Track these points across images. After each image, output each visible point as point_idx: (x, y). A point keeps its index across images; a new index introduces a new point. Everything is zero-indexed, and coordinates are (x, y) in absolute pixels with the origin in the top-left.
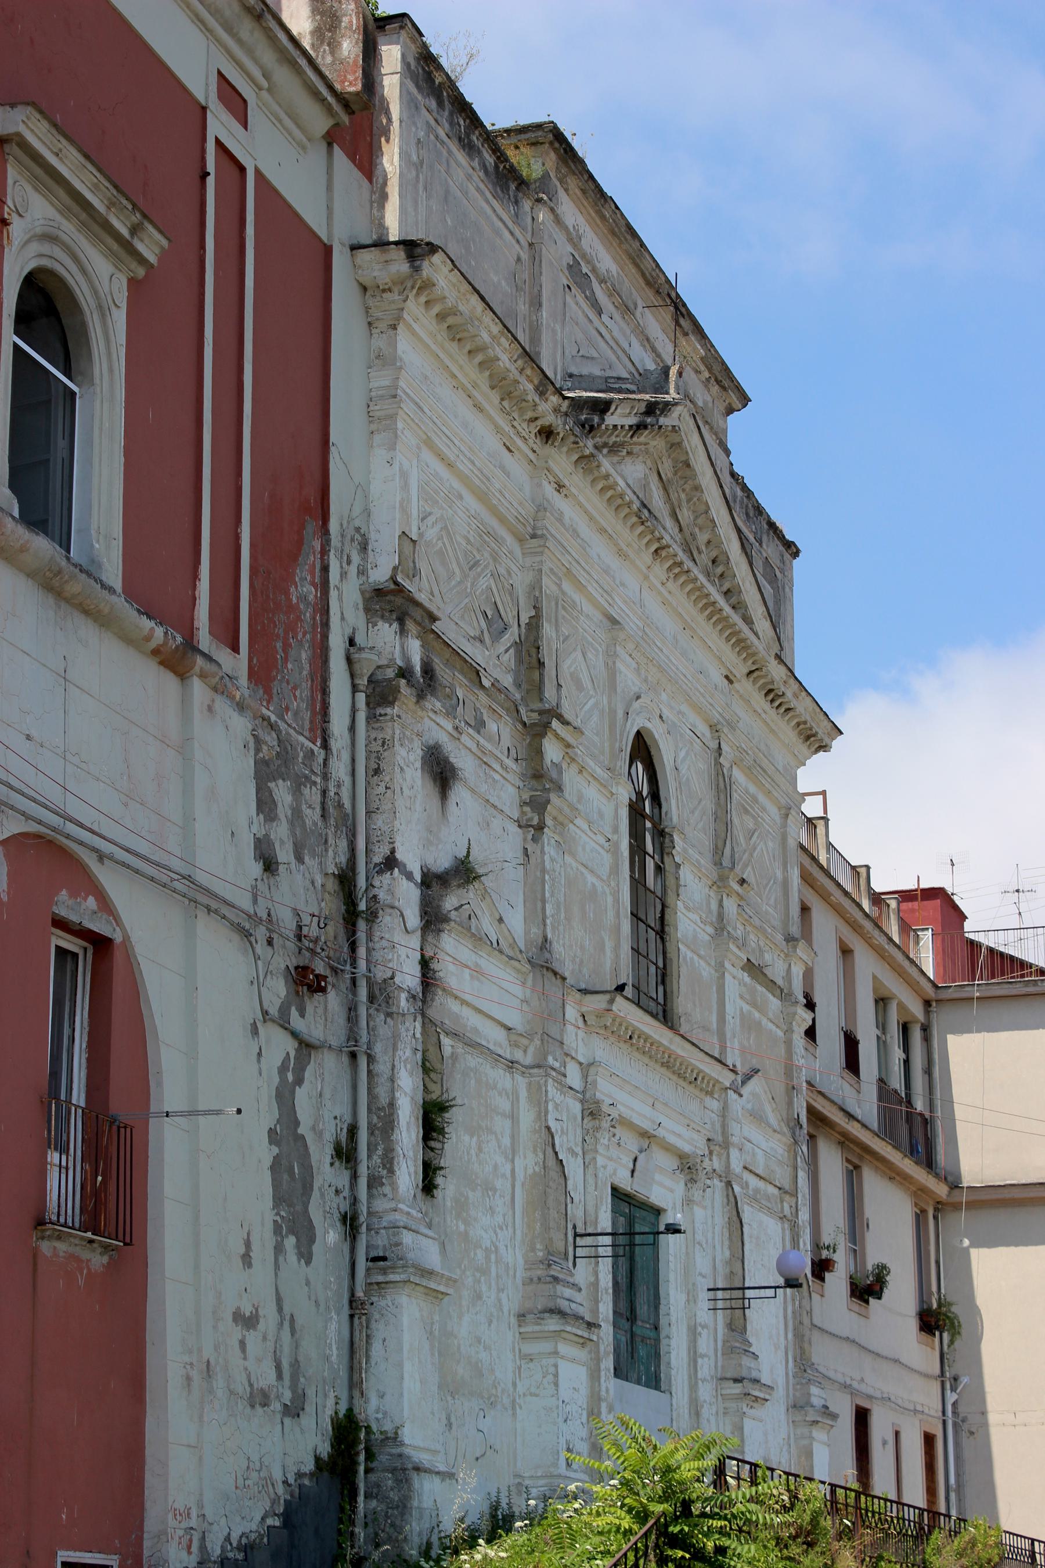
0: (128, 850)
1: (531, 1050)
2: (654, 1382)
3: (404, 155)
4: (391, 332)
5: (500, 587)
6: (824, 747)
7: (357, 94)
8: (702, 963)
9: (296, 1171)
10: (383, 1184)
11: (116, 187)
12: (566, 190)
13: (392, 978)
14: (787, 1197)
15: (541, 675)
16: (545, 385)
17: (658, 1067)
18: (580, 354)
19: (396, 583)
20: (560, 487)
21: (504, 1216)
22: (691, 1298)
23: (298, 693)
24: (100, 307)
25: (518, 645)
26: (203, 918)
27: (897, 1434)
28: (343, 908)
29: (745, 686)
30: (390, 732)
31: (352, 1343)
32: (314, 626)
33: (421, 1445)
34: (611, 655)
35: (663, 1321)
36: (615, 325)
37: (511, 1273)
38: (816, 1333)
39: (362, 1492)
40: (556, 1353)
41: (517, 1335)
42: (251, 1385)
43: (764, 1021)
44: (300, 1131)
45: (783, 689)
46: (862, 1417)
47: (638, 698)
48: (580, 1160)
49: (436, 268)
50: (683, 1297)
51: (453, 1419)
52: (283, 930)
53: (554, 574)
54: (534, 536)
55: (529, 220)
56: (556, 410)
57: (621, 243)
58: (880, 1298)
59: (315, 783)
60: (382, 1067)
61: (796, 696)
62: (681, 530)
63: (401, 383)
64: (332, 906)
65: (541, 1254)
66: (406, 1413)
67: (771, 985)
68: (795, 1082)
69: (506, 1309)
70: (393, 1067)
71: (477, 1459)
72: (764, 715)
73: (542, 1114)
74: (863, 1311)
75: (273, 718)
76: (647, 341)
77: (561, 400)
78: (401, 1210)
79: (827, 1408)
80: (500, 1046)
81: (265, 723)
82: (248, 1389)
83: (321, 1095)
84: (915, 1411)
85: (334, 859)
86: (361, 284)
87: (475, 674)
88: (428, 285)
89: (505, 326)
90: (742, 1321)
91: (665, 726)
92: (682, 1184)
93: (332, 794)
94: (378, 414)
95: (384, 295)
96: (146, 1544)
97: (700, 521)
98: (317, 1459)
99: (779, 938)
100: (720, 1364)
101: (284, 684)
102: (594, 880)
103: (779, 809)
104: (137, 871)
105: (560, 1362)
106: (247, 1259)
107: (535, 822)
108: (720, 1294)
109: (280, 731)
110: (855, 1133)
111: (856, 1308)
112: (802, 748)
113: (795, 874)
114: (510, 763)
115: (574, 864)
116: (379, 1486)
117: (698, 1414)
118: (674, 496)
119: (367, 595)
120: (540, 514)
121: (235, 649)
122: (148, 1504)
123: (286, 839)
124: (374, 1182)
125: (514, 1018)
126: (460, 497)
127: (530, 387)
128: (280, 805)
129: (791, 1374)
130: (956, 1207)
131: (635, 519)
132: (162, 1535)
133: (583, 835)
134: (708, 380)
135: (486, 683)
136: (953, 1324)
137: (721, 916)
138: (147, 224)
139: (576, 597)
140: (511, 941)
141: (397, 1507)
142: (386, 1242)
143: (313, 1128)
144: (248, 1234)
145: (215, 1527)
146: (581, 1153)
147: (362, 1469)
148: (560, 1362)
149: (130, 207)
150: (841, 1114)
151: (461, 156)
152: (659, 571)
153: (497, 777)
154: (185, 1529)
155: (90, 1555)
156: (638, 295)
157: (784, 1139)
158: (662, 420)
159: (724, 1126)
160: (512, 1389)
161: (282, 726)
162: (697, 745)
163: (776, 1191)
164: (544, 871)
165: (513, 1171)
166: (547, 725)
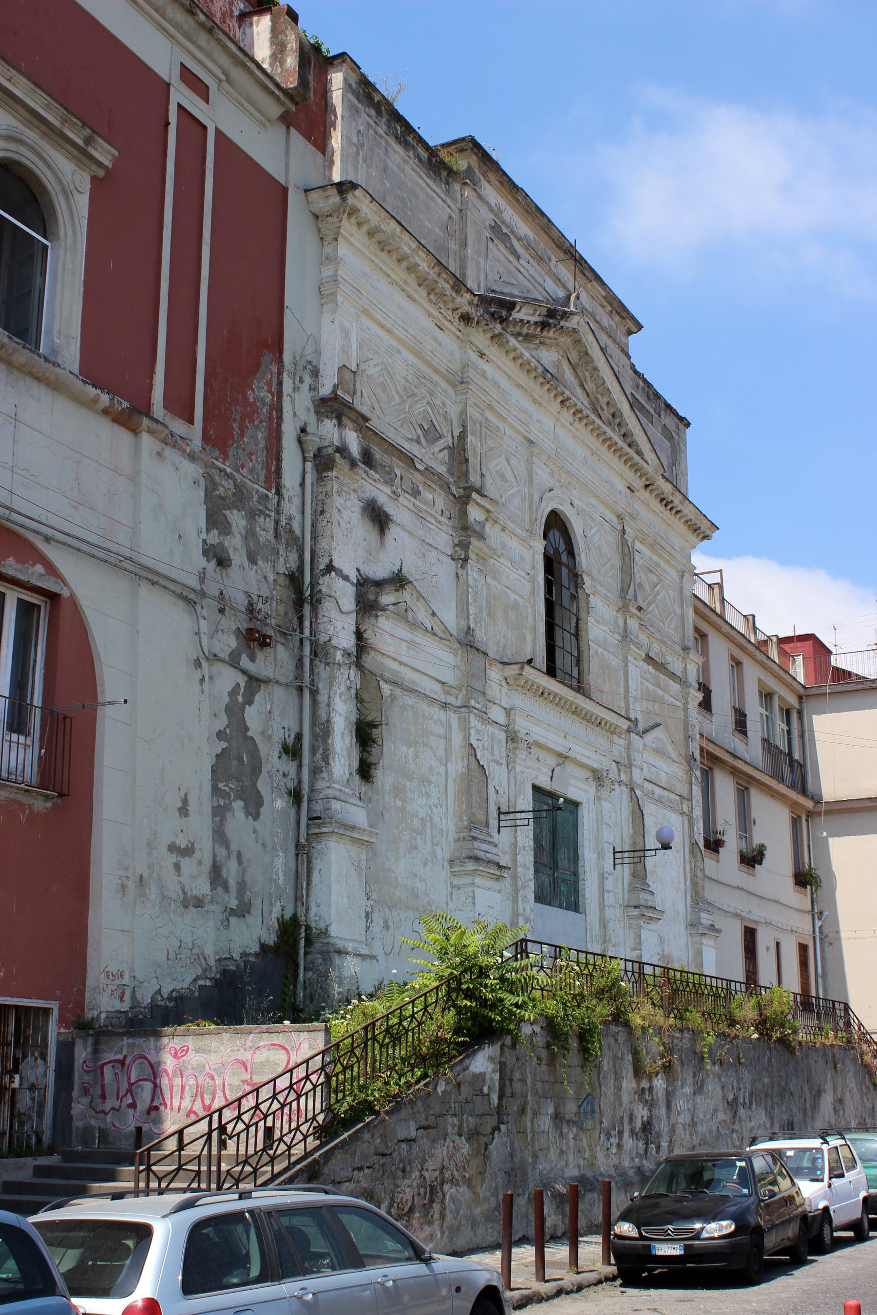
0: (66, 534)
1: (460, 697)
2: (574, 906)
3: (346, 138)
4: (335, 243)
5: (436, 411)
6: (706, 537)
7: (295, 88)
8: (611, 656)
9: (245, 759)
10: (322, 772)
11: (65, 109)
12: (489, 182)
13: (330, 641)
14: (685, 801)
15: (467, 467)
16: (458, 286)
17: (569, 714)
18: (502, 279)
19: (336, 395)
20: (482, 355)
21: (439, 799)
22: (600, 856)
23: (253, 458)
24: (64, 191)
25: (451, 449)
26: (145, 589)
27: (778, 944)
28: (293, 596)
29: (645, 495)
30: (330, 487)
31: (297, 872)
32: (270, 417)
33: (348, 937)
34: (529, 463)
35: (581, 870)
36: (534, 269)
37: (445, 834)
38: (707, 882)
39: (302, 967)
40: (473, 884)
41: (449, 873)
42: (184, 893)
43: (666, 696)
44: (249, 734)
45: (671, 498)
46: (750, 935)
47: (551, 490)
48: (504, 768)
49: (357, 199)
50: (595, 856)
51: (390, 923)
52: (235, 605)
53: (478, 406)
54: (462, 383)
55: (459, 196)
56: (470, 303)
57: (534, 219)
58: (761, 864)
59: (269, 516)
60: (322, 698)
61: (681, 502)
62: (588, 395)
63: (340, 273)
64: (283, 593)
65: (466, 823)
66: (333, 916)
67: (672, 675)
68: (690, 733)
69: (440, 857)
70: (329, 697)
71: (413, 949)
72: (661, 515)
73: (467, 736)
74: (750, 871)
75: (229, 470)
76: (558, 280)
77: (473, 297)
78: (334, 788)
79: (713, 926)
80: (436, 693)
81: (223, 473)
82: (182, 896)
83: (270, 713)
84: (792, 931)
85: (285, 564)
86: (314, 214)
87: (410, 461)
88: (353, 212)
89: (420, 243)
90: (643, 872)
91: (575, 510)
92: (594, 788)
93: (284, 524)
94: (326, 293)
95: (328, 219)
96: (87, 994)
97: (600, 390)
98: (263, 946)
99: (678, 648)
100: (626, 897)
101: (240, 451)
102: (517, 598)
103: (678, 572)
104: (79, 550)
105: (476, 890)
106: (184, 811)
107: (463, 556)
108: (626, 855)
109: (236, 480)
110: (740, 766)
111: (745, 870)
112: (693, 538)
113: (691, 611)
114: (443, 519)
115: (499, 586)
116: (313, 963)
117: (605, 927)
118: (580, 374)
119: (316, 403)
120: (466, 369)
121: (191, 421)
122: (89, 969)
123: (239, 547)
124: (315, 771)
125: (449, 676)
126: (400, 352)
127: (447, 286)
128: (234, 526)
129: (689, 906)
130: (819, 814)
131: (541, 380)
132: (96, 989)
133: (507, 569)
134: (611, 312)
135: (420, 467)
136: (816, 881)
137: (625, 629)
138: (96, 137)
139: (501, 426)
140: (443, 628)
141: (324, 976)
142: (322, 808)
143: (263, 733)
144: (186, 795)
145: (146, 985)
146: (505, 763)
147: (302, 952)
148: (476, 890)
149: (80, 124)
150: (725, 753)
151: (398, 148)
152: (567, 416)
153: (432, 527)
154: (118, 985)
155: (28, 1000)
156: (544, 246)
157: (682, 767)
158: (562, 323)
159: (629, 755)
160: (445, 906)
161: (238, 477)
162: (607, 527)
163: (678, 798)
164: (468, 586)
165: (446, 772)
166: (469, 497)
